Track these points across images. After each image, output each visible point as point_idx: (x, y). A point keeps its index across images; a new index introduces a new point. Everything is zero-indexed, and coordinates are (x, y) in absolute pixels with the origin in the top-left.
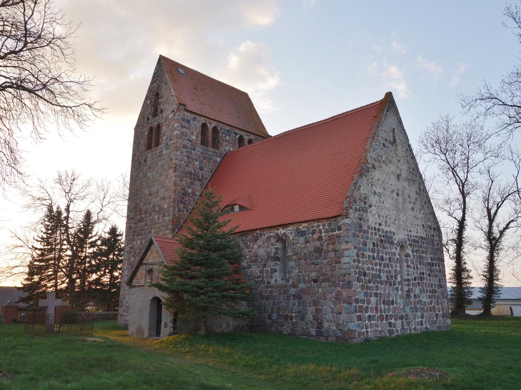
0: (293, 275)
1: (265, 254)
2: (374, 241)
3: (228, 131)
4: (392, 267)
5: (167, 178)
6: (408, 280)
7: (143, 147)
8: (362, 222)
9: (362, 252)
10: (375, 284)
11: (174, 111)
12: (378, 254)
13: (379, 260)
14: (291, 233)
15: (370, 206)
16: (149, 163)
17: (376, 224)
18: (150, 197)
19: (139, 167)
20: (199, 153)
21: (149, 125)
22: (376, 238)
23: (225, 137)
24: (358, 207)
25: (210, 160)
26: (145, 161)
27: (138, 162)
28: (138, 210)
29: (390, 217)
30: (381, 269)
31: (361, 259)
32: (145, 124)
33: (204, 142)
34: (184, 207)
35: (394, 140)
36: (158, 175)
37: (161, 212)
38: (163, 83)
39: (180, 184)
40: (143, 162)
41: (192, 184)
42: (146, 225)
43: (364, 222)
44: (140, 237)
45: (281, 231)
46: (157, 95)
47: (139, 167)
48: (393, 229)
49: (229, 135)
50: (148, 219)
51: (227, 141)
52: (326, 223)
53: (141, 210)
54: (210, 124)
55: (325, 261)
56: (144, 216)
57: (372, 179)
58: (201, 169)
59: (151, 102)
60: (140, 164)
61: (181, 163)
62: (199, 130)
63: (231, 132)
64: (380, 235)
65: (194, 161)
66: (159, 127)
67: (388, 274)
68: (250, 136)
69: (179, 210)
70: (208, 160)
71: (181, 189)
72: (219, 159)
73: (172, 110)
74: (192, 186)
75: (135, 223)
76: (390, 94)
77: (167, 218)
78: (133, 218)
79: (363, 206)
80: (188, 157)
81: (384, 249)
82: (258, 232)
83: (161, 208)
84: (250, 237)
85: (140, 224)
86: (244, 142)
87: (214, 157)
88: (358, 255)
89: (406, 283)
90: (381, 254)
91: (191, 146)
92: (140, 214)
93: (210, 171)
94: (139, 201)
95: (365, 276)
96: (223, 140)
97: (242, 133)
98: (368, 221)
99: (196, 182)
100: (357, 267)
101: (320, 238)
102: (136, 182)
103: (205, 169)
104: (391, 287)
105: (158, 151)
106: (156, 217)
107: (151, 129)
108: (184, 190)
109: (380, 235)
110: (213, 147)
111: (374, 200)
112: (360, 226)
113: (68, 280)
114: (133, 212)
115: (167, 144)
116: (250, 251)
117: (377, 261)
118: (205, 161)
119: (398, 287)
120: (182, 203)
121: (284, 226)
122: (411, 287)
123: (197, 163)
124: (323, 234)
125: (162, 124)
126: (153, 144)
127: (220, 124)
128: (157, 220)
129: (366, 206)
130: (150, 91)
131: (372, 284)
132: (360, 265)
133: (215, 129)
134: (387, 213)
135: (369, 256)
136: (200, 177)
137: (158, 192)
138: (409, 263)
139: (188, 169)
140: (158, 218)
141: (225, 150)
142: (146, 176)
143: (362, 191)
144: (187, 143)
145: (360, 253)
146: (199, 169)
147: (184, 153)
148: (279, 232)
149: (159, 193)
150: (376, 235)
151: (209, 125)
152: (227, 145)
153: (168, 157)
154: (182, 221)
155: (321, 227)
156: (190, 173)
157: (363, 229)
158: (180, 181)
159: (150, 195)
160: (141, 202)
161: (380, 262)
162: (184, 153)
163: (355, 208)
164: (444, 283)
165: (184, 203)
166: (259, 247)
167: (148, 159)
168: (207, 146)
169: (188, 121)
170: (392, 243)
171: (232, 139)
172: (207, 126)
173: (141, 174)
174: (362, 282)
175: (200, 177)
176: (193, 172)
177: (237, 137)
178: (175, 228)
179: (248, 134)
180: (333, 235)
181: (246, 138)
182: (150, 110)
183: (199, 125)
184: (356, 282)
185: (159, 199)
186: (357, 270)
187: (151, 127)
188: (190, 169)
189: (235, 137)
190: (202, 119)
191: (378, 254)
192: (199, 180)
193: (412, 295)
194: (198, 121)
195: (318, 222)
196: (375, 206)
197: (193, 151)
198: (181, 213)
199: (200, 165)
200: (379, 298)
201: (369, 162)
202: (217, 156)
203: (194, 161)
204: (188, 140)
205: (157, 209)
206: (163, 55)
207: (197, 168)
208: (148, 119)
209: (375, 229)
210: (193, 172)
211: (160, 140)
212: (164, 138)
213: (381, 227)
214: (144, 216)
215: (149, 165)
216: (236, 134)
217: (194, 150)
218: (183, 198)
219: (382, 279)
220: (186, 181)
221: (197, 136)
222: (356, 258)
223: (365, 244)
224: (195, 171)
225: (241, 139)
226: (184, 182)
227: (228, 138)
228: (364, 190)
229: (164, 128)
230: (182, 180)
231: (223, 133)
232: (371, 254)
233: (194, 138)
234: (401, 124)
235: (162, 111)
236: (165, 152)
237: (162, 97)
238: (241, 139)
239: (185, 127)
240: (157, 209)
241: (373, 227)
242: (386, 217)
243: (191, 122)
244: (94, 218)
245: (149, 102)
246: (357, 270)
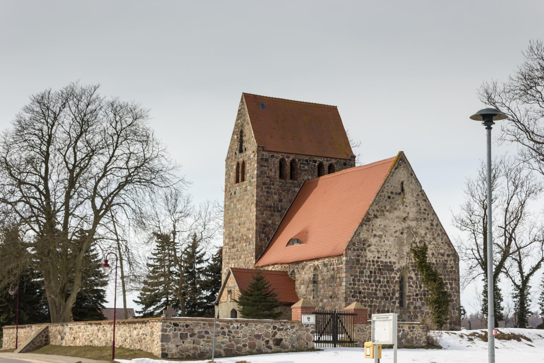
0: (321, 293)
1: (308, 278)
2: (371, 270)
3: (307, 161)
4: (389, 287)
5: (251, 212)
6: (409, 296)
7: (233, 180)
8: (360, 258)
9: (358, 278)
10: (370, 299)
11: (254, 152)
12: (375, 277)
13: (375, 283)
14: (321, 265)
15: (369, 246)
16: (238, 195)
17: (374, 257)
18: (239, 227)
19: (231, 198)
20: (278, 187)
21: (237, 160)
22: (373, 268)
23: (304, 167)
24: (356, 248)
25: (289, 191)
26: (235, 193)
27: (230, 193)
28: (231, 237)
29: (390, 251)
30: (378, 288)
31: (357, 283)
32: (234, 158)
33: (282, 176)
34: (265, 237)
35: (403, 190)
36: (245, 208)
37: (247, 240)
38: (246, 122)
39: (261, 218)
40: (233, 194)
41: (272, 215)
42: (238, 251)
43: (362, 257)
44: (234, 261)
45: (316, 263)
46: (242, 132)
47: (231, 198)
48: (393, 260)
49: (308, 164)
50: (239, 246)
51: (305, 170)
52: (336, 259)
53: (233, 238)
54: (288, 157)
55: (335, 285)
56: (235, 243)
57: (373, 225)
58: (280, 201)
59: (238, 138)
60: (231, 195)
61: (261, 199)
62: (277, 166)
63: (310, 161)
64: (379, 266)
65: (273, 195)
66: (244, 163)
67: (385, 292)
68: (330, 160)
69: (261, 240)
70: (286, 191)
71: (262, 221)
72: (297, 190)
73: (253, 151)
74: (272, 217)
75: (229, 249)
76: (402, 154)
77: (251, 246)
78: (228, 244)
79: (362, 246)
80: (268, 192)
81: (383, 274)
82: (305, 262)
83: (248, 238)
84: (300, 266)
85: (233, 249)
86: (324, 168)
87: (293, 188)
88: (354, 280)
89: (408, 298)
90: (378, 279)
91: (270, 182)
92: (233, 241)
93: (288, 202)
94: (231, 230)
95: (361, 294)
96: (301, 170)
97: (321, 160)
98: (366, 256)
99: (276, 213)
100: (352, 288)
101: (333, 269)
102: (229, 211)
103: (284, 200)
104: (387, 301)
105: (244, 187)
106: (244, 244)
107: (238, 164)
108: (264, 221)
109: (379, 266)
110: (291, 178)
111: (373, 241)
112: (358, 261)
113: (69, 238)
114: (227, 239)
115: (250, 181)
116: (300, 276)
117: (374, 284)
118: (283, 193)
119: (395, 301)
120: (263, 233)
121: (317, 259)
122: (412, 300)
123: (276, 197)
124: (335, 266)
125: (246, 161)
126: (240, 179)
127: (298, 156)
128: (245, 248)
129: (365, 246)
130: (236, 127)
131: (366, 299)
132: (356, 286)
133: (293, 162)
134: (387, 248)
135: (366, 281)
136: (280, 209)
137: (245, 223)
138: (411, 283)
139: (268, 203)
140: (246, 246)
141: (304, 180)
142: (236, 207)
143: (361, 236)
144: (267, 180)
145: (356, 279)
146: (278, 201)
147: (264, 189)
148: (315, 263)
149: (246, 224)
150: (374, 265)
151: (287, 159)
152: (305, 174)
153: (251, 193)
154: (264, 248)
155: (334, 262)
156: (270, 207)
157: (361, 262)
158: (261, 214)
159: (240, 224)
160: (233, 230)
161: (377, 284)
162: (264, 189)
163: (354, 249)
164: (456, 298)
165: (265, 233)
166: (305, 273)
167: (237, 192)
168: (285, 179)
169: (267, 160)
170: (392, 270)
171: (311, 168)
172: (285, 161)
173: (232, 205)
174: (357, 298)
175: (280, 209)
176: (272, 205)
177: (316, 164)
178: (258, 255)
179: (329, 159)
180: (339, 267)
181: (326, 164)
182: (236, 146)
183: (277, 161)
184: (351, 298)
185: (246, 229)
186: (353, 290)
187: (238, 162)
188: (270, 203)
189: (315, 166)
190: (280, 155)
191: (375, 277)
192: (278, 211)
193: (412, 307)
194: (276, 158)
195: (333, 258)
196: (375, 245)
197: (272, 186)
198: (263, 242)
199: (279, 197)
200: (373, 308)
201: (371, 214)
202: (295, 187)
203: (273, 195)
204: (267, 177)
205: (245, 237)
206: (245, 92)
207: (276, 201)
208: (236, 153)
209: (373, 261)
210: (272, 205)
211: (245, 176)
212: (248, 175)
213: (379, 260)
214: (235, 243)
215: (238, 197)
216: (315, 162)
217: (273, 184)
218: (264, 229)
219: (378, 296)
220: (266, 214)
221: (275, 172)
222: (352, 282)
223: (362, 272)
224: (274, 204)
225: (321, 166)
226: (264, 215)
227: (306, 167)
228: (363, 235)
229: (247, 165)
230: (262, 214)
231: (301, 164)
232: (367, 279)
233: (272, 174)
234: (412, 175)
235: (246, 150)
236: (249, 188)
237: (245, 135)
238: (321, 166)
239: (265, 166)
240: (245, 237)
241: (371, 261)
242: (387, 252)
243: (269, 160)
244: (198, 239)
245: (236, 137)
246: (353, 290)
